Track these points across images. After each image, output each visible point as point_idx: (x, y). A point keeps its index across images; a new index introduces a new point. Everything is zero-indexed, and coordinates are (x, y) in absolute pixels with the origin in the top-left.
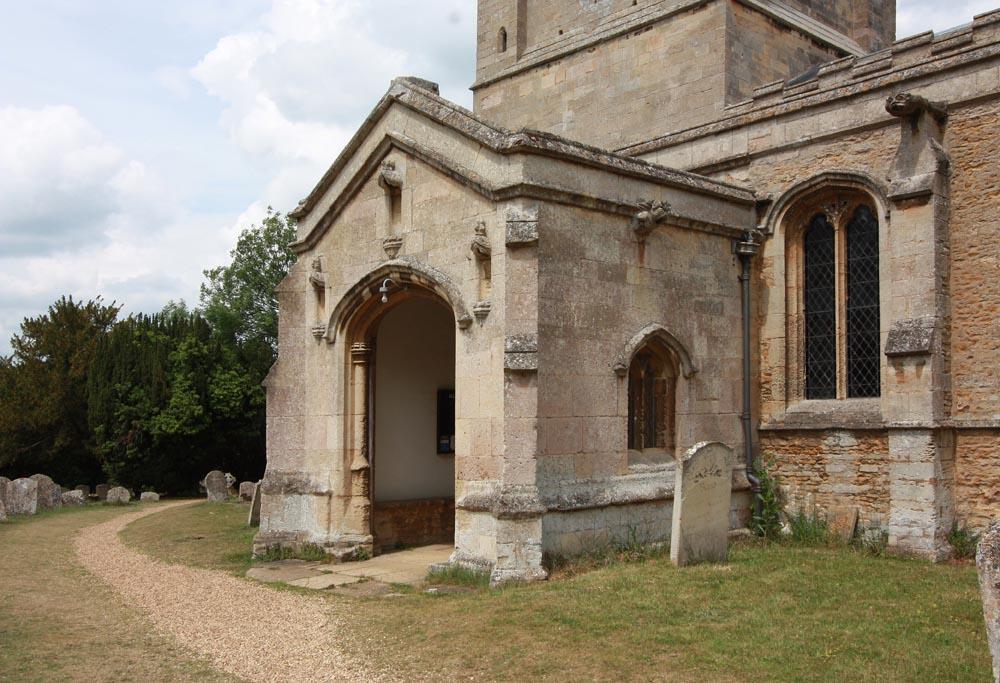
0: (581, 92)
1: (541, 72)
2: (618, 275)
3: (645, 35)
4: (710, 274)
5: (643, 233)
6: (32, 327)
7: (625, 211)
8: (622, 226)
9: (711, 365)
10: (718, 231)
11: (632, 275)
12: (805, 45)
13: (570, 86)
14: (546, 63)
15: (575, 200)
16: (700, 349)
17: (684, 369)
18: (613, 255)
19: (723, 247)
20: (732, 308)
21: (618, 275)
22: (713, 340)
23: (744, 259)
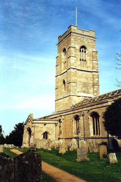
0: (62, 103)
2: (42, 128)
5: (45, 124)
6: (16, 125)
8: (43, 124)
9: (52, 134)
10: (53, 123)
11: (44, 127)
12: (83, 98)
13: (62, 102)
14: (60, 99)
15: (38, 123)
16: (51, 132)
17: (49, 134)
18: (42, 126)
19: (54, 124)
22: (52, 131)
23: (56, 125)
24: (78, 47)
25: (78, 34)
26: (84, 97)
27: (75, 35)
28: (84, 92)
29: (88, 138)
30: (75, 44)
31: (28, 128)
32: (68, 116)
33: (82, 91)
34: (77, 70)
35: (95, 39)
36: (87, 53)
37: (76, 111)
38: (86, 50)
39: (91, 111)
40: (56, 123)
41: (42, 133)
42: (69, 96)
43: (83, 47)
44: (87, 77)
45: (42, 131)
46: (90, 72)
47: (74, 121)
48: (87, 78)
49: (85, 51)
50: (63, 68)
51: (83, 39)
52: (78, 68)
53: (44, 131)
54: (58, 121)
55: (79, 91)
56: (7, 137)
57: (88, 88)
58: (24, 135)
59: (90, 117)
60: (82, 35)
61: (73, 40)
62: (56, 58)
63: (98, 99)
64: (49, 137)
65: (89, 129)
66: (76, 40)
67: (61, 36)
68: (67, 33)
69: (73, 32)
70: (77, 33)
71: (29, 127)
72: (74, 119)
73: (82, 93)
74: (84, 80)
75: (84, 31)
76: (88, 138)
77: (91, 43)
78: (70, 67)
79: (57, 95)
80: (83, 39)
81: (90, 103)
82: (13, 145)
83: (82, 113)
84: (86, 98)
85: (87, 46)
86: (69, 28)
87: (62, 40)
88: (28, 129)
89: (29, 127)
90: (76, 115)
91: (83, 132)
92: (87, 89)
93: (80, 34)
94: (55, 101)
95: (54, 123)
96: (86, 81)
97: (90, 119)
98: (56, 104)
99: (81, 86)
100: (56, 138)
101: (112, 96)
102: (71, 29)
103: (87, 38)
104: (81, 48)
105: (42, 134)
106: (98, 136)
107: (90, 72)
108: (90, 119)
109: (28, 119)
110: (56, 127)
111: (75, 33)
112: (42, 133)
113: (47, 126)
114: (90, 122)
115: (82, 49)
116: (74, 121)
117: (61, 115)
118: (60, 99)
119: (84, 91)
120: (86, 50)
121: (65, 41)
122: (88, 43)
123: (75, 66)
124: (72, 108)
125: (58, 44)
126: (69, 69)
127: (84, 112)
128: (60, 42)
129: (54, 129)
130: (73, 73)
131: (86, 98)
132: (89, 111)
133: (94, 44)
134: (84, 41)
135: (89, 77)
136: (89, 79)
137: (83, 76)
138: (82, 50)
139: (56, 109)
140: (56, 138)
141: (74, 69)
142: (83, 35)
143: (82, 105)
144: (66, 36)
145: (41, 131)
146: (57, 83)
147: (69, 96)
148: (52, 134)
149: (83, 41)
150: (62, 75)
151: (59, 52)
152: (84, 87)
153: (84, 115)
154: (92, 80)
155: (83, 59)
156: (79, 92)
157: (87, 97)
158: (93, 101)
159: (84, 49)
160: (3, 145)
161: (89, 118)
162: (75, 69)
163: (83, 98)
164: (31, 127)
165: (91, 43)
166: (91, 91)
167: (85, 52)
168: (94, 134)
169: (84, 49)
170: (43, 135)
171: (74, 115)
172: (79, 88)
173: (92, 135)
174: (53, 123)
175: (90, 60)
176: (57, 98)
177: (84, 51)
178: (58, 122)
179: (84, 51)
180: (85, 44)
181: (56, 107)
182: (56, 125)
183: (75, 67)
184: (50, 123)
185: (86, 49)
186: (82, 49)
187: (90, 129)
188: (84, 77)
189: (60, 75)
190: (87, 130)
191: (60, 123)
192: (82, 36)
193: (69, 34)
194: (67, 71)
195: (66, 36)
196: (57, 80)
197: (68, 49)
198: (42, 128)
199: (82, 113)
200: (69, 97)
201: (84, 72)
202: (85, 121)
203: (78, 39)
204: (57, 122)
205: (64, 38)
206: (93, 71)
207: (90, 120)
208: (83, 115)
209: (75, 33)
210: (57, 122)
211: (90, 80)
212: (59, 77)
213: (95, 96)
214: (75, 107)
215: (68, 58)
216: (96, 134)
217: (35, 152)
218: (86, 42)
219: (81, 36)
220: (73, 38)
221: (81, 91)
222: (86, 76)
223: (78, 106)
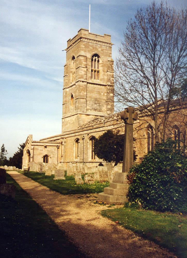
1: (67, 118)
3: (73, 116)
4: (53, 149)
5: (46, 147)
7: (43, 146)
8: (43, 147)
9: (53, 157)
10: (54, 146)
11: (44, 150)
14: (67, 117)
16: (52, 156)
17: (50, 157)
19: (55, 147)
20: (56, 152)
21: (42, 150)
22: (53, 155)
23: (58, 148)
24: (89, 56)
25: (90, 39)
26: (95, 116)
27: (86, 40)
28: (95, 110)
29: (87, 162)
30: (85, 51)
31: (27, 150)
32: (70, 138)
33: (92, 108)
34: (88, 83)
35: (110, 46)
36: (100, 62)
37: (77, 134)
38: (100, 59)
39: (90, 135)
40: (58, 146)
41: (42, 156)
42: (77, 114)
43: (96, 55)
44: (99, 92)
45: (41, 154)
46: (103, 85)
47: (75, 144)
48: (99, 93)
49: (98, 60)
50: (72, 80)
51: (96, 46)
52: (89, 81)
53: (45, 154)
54: (60, 143)
55: (89, 108)
56: (11, 158)
57: (100, 105)
58: (23, 157)
59: (89, 141)
60: (95, 40)
61: (84, 46)
62: (64, 66)
63: (104, 121)
64: (50, 160)
65: (87, 153)
66: (87, 46)
67: (71, 39)
68: (77, 38)
69: (84, 37)
70: (88, 39)
71: (28, 149)
72: (75, 142)
73: (92, 110)
74: (95, 95)
75: (97, 36)
76: (87, 162)
77: (106, 50)
78: (79, 80)
79: (65, 113)
80: (96, 46)
81: (96, 124)
82: (15, 167)
83: (82, 137)
84: (97, 117)
85: (100, 54)
86: (79, 32)
87: (71, 45)
88: (27, 151)
89: (28, 149)
90: (77, 138)
91: (83, 156)
92: (99, 106)
93: (93, 40)
94: (62, 119)
95: (56, 146)
96: (97, 96)
97: (89, 143)
98: (63, 122)
99: (91, 103)
100: (58, 161)
101: (117, 118)
102: (81, 34)
103: (101, 44)
104: (93, 57)
105: (42, 158)
106: (94, 161)
107: (103, 85)
108: (89, 143)
109: (27, 140)
110: (58, 150)
111: (86, 38)
112: (42, 157)
113: (48, 148)
114: (89, 146)
115: (94, 57)
116: (75, 144)
117: (62, 137)
118: (67, 117)
119: (96, 109)
120: (100, 59)
121: (74, 47)
122: (102, 50)
123: (85, 78)
124: (79, 128)
125: (67, 49)
126: (77, 82)
127: (84, 135)
128: (69, 47)
129: (56, 152)
130: (82, 86)
131: (97, 117)
132: (88, 134)
133: (109, 52)
134: (98, 47)
135: (102, 92)
136: (102, 94)
137: (95, 90)
138: (94, 59)
139: (62, 128)
140: (58, 161)
141: (83, 82)
142: (97, 41)
143: (89, 126)
144: (76, 41)
145: (40, 154)
146: (65, 97)
147: (77, 114)
148: (53, 157)
149: (96, 48)
150: (72, 87)
151: (68, 59)
152: (95, 104)
153: (84, 139)
154: (105, 96)
155: (95, 69)
156: (89, 109)
157: (98, 116)
158: (100, 122)
159: (97, 57)
160: (4, 166)
161: (88, 142)
162: (85, 82)
163: (94, 117)
164: (30, 150)
165: (106, 50)
166: (104, 108)
167: (98, 61)
168: (92, 158)
169: (97, 57)
170: (43, 158)
171: (76, 137)
172: (89, 105)
173: (90, 159)
174: (54, 146)
175: (104, 71)
176: (64, 115)
177: (97, 59)
178: (61, 145)
179: (97, 59)
180: (99, 51)
181: (62, 126)
182: (58, 148)
183: (84, 79)
184: (50, 146)
185: (100, 57)
186: (94, 57)
187: (89, 153)
188: (96, 92)
189: (68, 88)
190: (86, 154)
191: (78, 143)
192: (95, 42)
193: (78, 40)
194: (75, 84)
195: (76, 41)
196: (65, 94)
197: (77, 57)
198: (42, 150)
199: (82, 137)
200: (77, 115)
201: (95, 86)
202: (85, 144)
203: (89, 45)
204: (59, 145)
205: (73, 44)
206: (107, 84)
207: (89, 144)
208: (83, 139)
209: (86, 38)
210: (59, 145)
211: (104, 95)
212: (68, 90)
213: (109, 114)
214: (82, 128)
215: (77, 69)
216: (93, 158)
217: (155, 179)
218: (100, 50)
219: (93, 42)
220: (84, 45)
221: (91, 108)
222: (99, 91)
223: (85, 127)
